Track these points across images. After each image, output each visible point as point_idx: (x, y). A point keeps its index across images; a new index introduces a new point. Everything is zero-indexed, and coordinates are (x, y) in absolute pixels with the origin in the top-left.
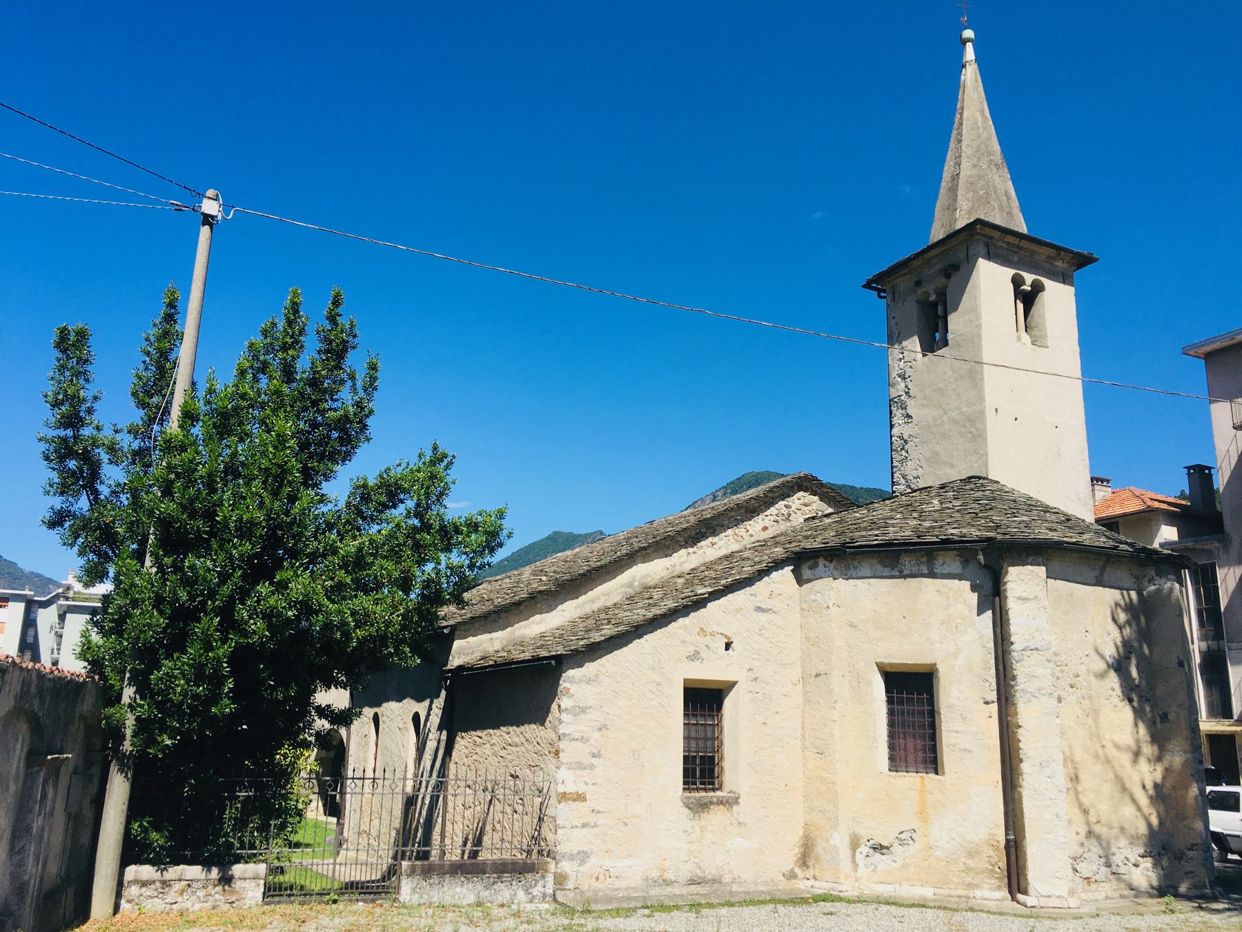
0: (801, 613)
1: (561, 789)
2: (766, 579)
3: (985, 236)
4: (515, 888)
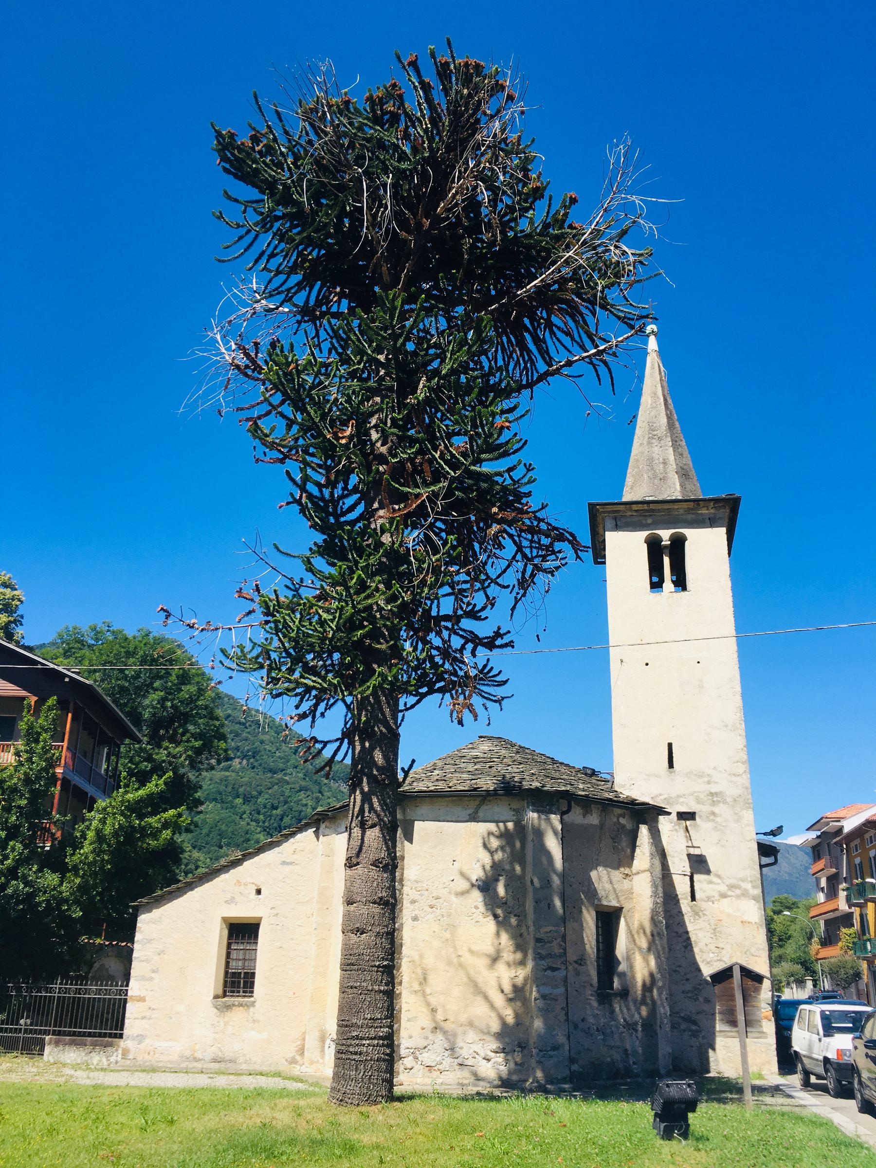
2: (292, 840)
3: (609, 512)
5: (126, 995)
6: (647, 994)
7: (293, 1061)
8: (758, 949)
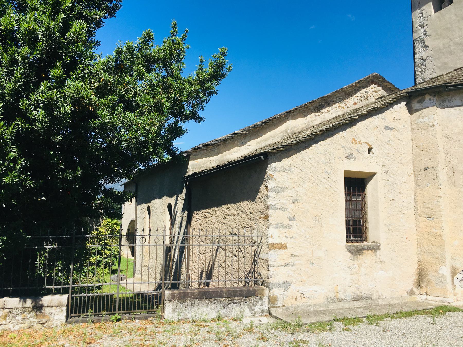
0: (412, 131)
1: (270, 241)
2: (391, 109)
4: (243, 306)
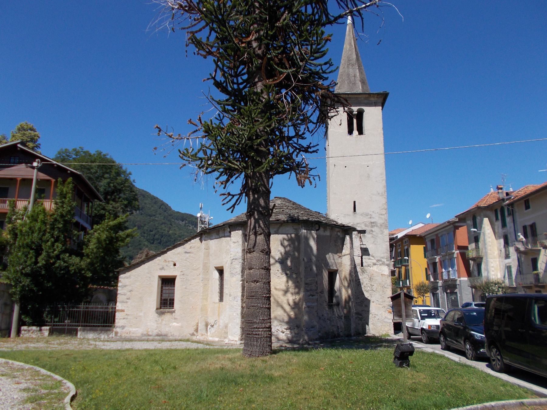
2: (189, 243)
5: (115, 309)
6: (347, 304)
7: (193, 335)
8: (388, 285)
